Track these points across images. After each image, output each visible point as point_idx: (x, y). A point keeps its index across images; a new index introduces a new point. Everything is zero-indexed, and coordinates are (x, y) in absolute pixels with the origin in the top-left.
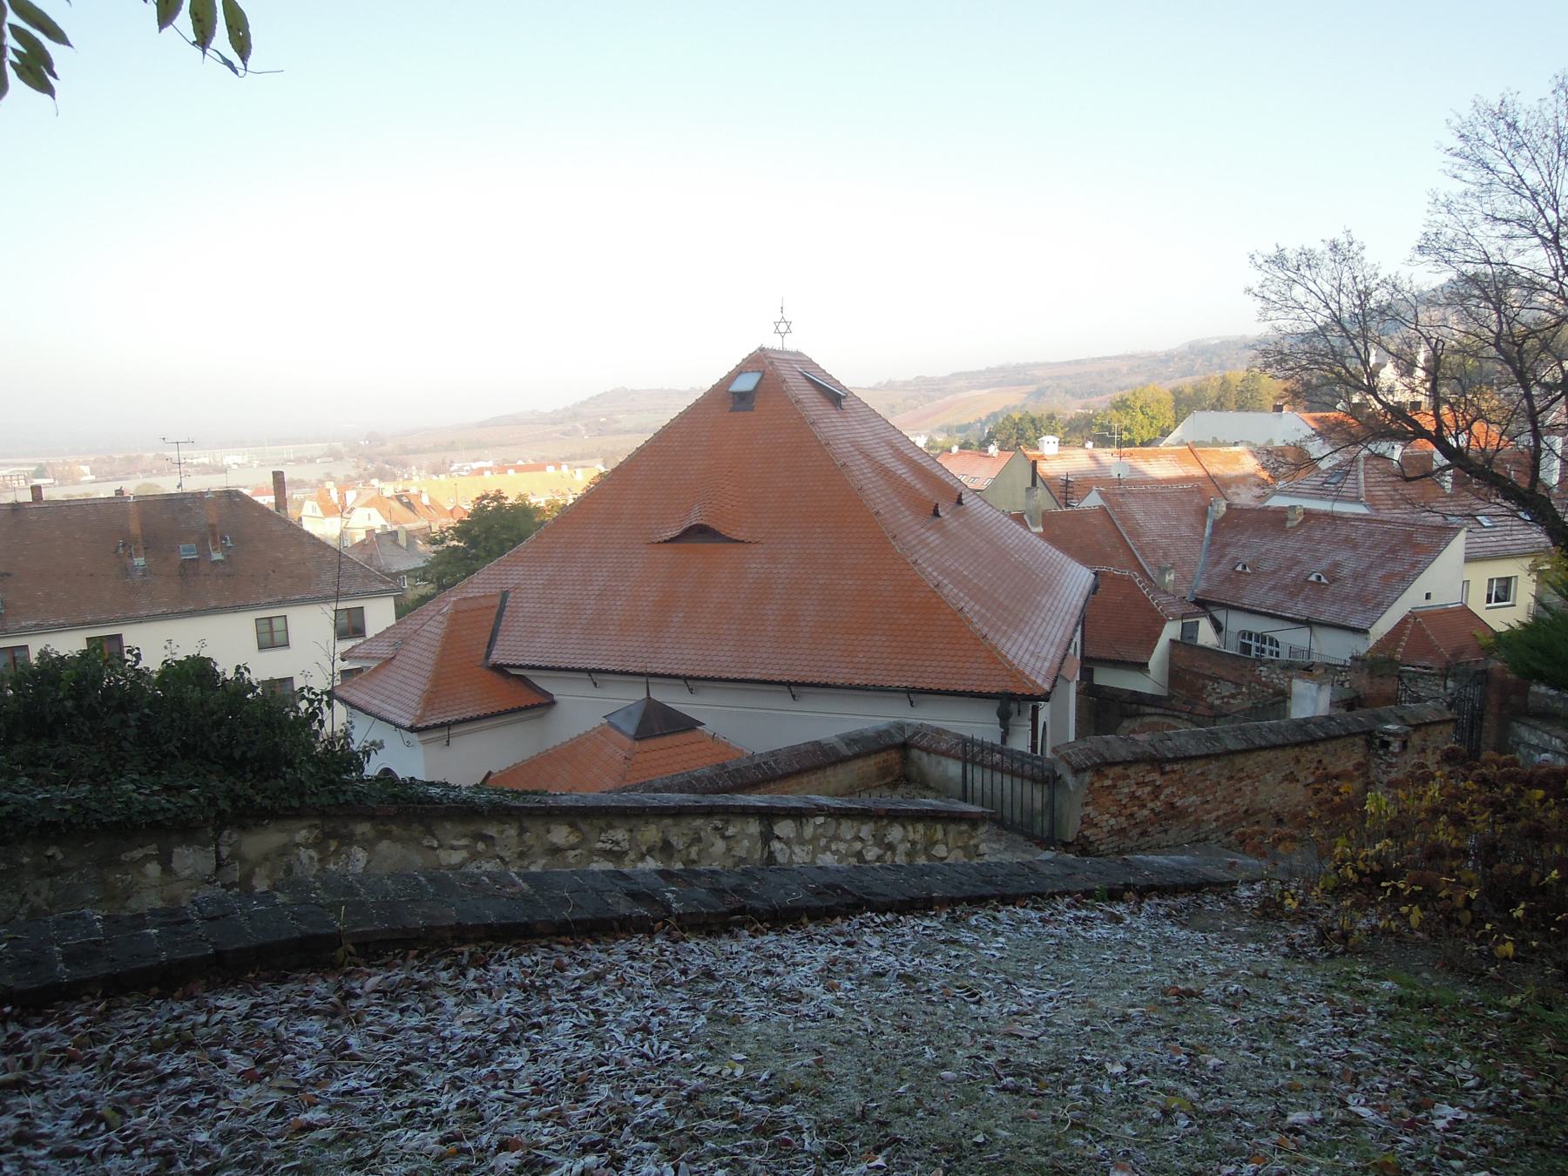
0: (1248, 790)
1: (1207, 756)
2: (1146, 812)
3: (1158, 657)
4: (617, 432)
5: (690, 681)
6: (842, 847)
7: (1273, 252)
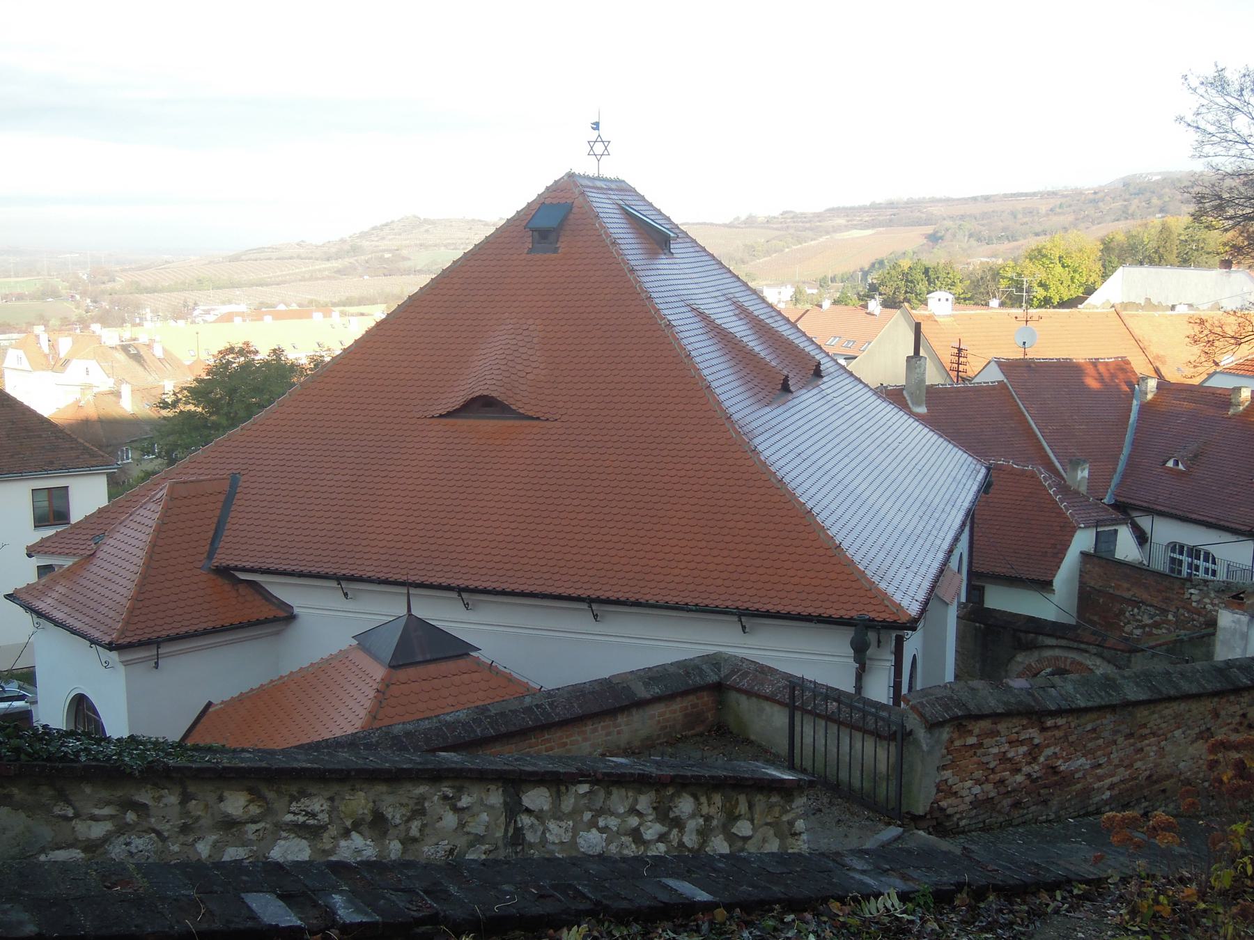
0: (1151, 752)
1: (1100, 708)
2: (1019, 778)
3: (1066, 574)
4: (408, 272)
5: (466, 592)
6: (613, 823)
7: (1211, 73)
